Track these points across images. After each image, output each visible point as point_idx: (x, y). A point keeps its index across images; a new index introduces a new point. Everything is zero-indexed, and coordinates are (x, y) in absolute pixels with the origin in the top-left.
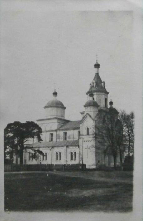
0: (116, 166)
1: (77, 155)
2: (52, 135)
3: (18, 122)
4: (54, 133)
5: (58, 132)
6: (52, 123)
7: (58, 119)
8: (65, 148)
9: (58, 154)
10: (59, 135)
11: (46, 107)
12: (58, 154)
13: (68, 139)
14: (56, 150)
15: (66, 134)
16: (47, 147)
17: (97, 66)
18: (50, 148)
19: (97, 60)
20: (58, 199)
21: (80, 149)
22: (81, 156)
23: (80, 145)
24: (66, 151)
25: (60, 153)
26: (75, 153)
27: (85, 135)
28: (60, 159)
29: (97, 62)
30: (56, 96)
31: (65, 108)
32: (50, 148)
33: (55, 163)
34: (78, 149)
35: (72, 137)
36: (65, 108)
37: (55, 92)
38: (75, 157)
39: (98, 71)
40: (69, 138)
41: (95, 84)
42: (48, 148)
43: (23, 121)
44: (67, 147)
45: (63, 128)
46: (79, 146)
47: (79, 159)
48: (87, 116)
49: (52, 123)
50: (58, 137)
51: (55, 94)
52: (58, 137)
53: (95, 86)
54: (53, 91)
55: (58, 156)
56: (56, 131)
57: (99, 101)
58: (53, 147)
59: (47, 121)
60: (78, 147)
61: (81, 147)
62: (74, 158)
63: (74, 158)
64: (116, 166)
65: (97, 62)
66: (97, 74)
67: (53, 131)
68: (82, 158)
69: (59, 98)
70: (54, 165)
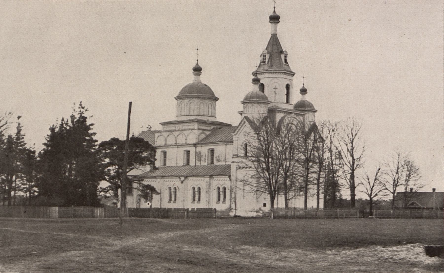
0: (133, 189)
1: (228, 192)
2: (188, 152)
3: (118, 139)
4: (192, 150)
5: (199, 149)
6: (189, 130)
7: (198, 121)
8: (207, 179)
9: (196, 190)
10: (200, 153)
11: (178, 98)
12: (196, 190)
13: (216, 163)
14: (193, 182)
15: (212, 151)
16: (176, 176)
17: (275, 19)
18: (182, 179)
19: (275, 8)
20: (68, 166)
21: (231, 182)
22: (233, 195)
23: (231, 174)
24: (210, 184)
25: (199, 188)
26: (225, 188)
27: (241, 157)
28: (199, 200)
29: (274, 12)
30: (199, 75)
31: (216, 99)
32: (182, 179)
33: (190, 206)
34: (230, 182)
35: (223, 159)
36: (216, 99)
37: (197, 67)
38: (225, 197)
39: (276, 30)
40: (218, 161)
41: (268, 56)
42: (178, 179)
43: (145, 140)
44: (211, 176)
45: (212, 140)
46: (230, 176)
47: (231, 200)
48: (245, 122)
49: (189, 130)
50: (199, 156)
51: (197, 70)
52: (199, 156)
53: (267, 61)
54: (194, 65)
55: (196, 193)
56: (195, 145)
57: (274, 90)
58: (186, 177)
59: (180, 126)
60: (228, 179)
61: (233, 178)
62: (222, 198)
63: (222, 198)
64: (133, 189)
65: (274, 12)
66: (274, 40)
67: (187, 145)
68: (235, 198)
69: (204, 79)
70: (195, 210)
